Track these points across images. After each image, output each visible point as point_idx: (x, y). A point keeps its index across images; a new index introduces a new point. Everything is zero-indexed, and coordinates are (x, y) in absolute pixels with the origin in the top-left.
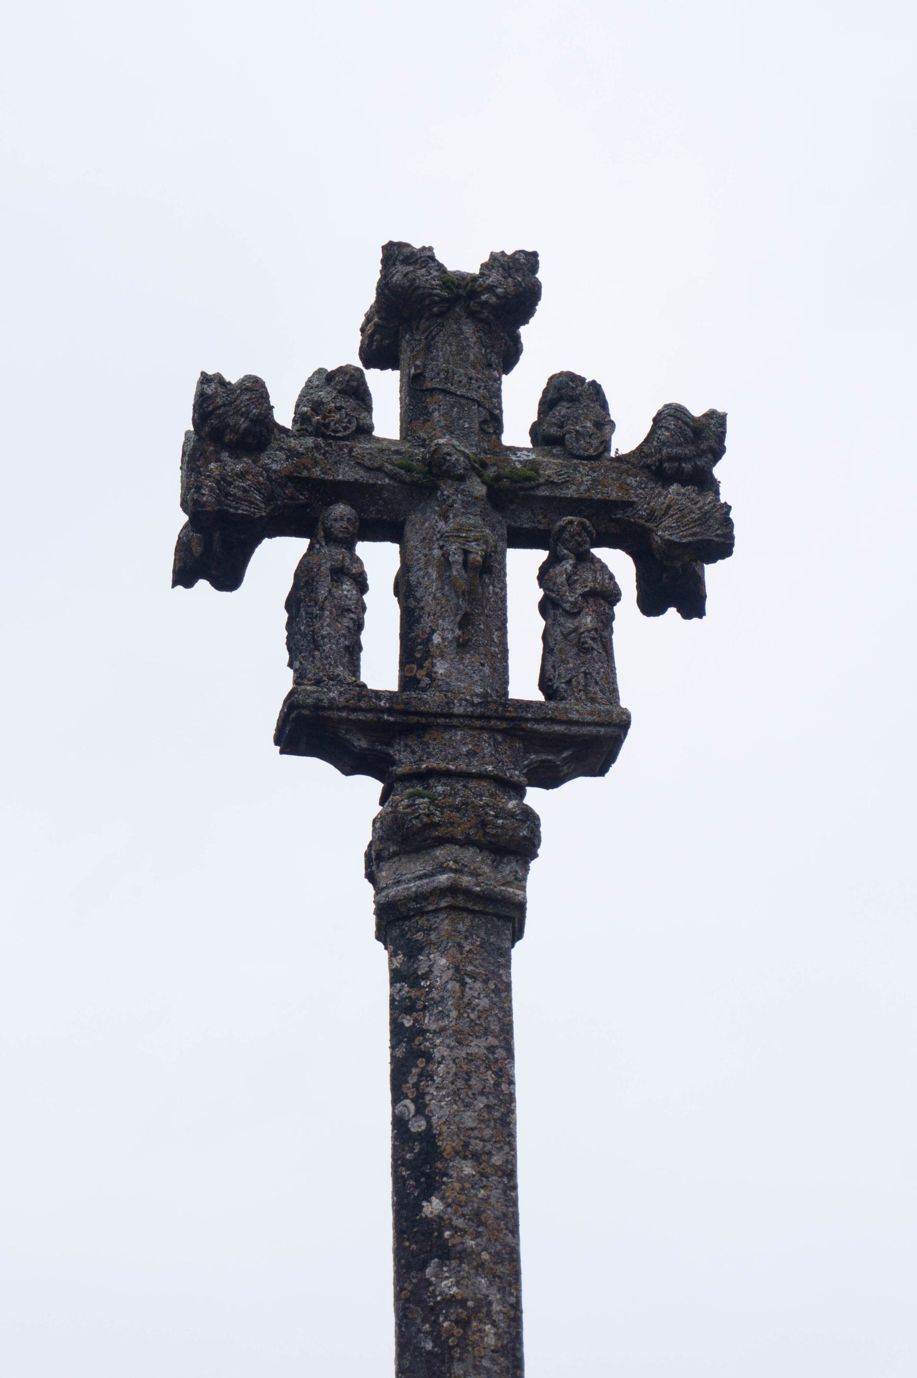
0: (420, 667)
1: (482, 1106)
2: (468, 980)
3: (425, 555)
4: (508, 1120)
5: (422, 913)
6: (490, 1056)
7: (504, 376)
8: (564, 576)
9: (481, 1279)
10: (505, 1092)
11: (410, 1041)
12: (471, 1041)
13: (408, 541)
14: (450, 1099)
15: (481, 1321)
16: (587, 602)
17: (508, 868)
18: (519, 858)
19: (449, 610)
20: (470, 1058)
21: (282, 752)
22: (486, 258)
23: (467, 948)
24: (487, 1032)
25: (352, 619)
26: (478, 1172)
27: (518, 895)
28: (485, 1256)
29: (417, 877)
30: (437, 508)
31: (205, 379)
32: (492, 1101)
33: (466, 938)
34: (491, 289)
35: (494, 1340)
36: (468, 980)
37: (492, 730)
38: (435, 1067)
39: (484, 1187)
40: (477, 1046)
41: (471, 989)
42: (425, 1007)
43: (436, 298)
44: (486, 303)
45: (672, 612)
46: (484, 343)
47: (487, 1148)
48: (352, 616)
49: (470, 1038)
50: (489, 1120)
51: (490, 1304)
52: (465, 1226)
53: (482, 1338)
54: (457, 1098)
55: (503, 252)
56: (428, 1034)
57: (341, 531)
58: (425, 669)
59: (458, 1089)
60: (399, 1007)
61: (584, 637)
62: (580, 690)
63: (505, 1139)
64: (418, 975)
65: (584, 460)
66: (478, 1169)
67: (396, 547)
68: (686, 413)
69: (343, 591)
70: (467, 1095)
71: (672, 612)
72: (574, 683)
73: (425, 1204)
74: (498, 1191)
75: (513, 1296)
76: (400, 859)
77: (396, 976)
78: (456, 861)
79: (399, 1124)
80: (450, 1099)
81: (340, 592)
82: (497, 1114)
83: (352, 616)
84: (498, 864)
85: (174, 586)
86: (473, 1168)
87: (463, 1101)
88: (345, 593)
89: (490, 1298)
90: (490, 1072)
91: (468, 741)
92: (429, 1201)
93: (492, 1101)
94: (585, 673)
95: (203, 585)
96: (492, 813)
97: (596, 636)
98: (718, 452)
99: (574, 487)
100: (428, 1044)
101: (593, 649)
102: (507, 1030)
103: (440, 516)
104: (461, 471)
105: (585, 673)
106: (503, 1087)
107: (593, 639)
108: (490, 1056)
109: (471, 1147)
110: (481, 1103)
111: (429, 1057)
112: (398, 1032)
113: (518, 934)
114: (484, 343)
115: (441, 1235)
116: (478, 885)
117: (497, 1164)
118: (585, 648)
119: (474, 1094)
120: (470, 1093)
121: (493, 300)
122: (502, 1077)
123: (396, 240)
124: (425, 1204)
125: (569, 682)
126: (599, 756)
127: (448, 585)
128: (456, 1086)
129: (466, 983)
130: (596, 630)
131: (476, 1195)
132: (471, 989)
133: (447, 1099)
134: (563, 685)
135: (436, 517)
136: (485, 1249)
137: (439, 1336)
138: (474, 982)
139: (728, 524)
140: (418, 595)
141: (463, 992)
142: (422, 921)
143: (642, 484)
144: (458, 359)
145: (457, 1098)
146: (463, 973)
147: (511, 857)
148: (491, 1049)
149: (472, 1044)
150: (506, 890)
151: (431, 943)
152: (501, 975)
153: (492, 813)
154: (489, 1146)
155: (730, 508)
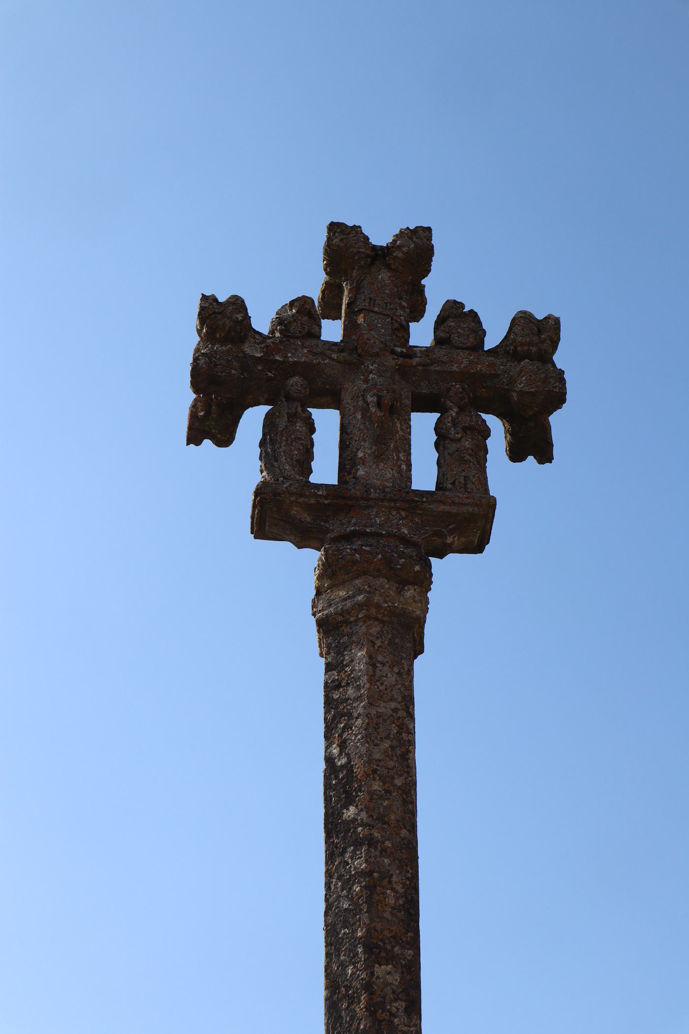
0: (349, 473)
1: (387, 745)
2: (379, 665)
3: (354, 406)
4: (407, 757)
5: (347, 622)
6: (395, 714)
7: (413, 326)
8: (450, 418)
9: (384, 859)
10: (404, 739)
11: (337, 707)
12: (380, 704)
13: (343, 400)
14: (363, 740)
15: (383, 887)
16: (466, 434)
17: (410, 592)
18: (416, 587)
19: (369, 436)
20: (379, 715)
21: (255, 538)
22: (397, 232)
23: (379, 645)
24: (392, 699)
25: (302, 444)
26: (384, 790)
27: (416, 612)
28: (388, 844)
29: (343, 600)
30: (362, 377)
31: (204, 298)
32: (395, 743)
33: (378, 638)
34: (400, 247)
35: (393, 900)
36: (379, 665)
37: (398, 509)
38: (354, 721)
39: (388, 799)
40: (385, 708)
41: (380, 670)
42: (348, 684)
43: (362, 255)
44: (396, 257)
45: (531, 459)
46: (396, 285)
47: (390, 774)
48: (302, 442)
49: (380, 702)
50: (392, 756)
51: (392, 876)
52: (373, 823)
53: (385, 898)
54: (368, 740)
55: (408, 228)
56: (349, 701)
57: (296, 392)
58: (352, 474)
59: (370, 734)
60: (329, 688)
61: (463, 453)
62: (461, 488)
63: (404, 768)
64: (343, 665)
65: (464, 350)
66: (383, 788)
67: (338, 412)
68: (531, 319)
69: (296, 427)
70: (376, 738)
71: (531, 459)
72: (457, 483)
73: (345, 811)
74: (398, 802)
75: (409, 873)
76: (332, 590)
77: (329, 668)
78: (369, 586)
79: (329, 760)
80: (363, 740)
81: (294, 428)
82: (398, 752)
83: (302, 442)
84: (401, 591)
85: (188, 444)
86: (379, 786)
87: (373, 741)
88: (298, 428)
89: (391, 873)
90: (394, 725)
91: (381, 515)
92: (348, 809)
93: (395, 743)
94: (465, 477)
95: (207, 443)
96: (395, 555)
97: (473, 453)
98: (555, 343)
99: (456, 365)
100: (349, 707)
101: (470, 461)
102: (409, 700)
103: (363, 382)
104: (377, 350)
105: (465, 477)
106: (403, 735)
107: (470, 455)
108: (395, 714)
109: (378, 773)
110: (386, 744)
111: (350, 715)
112: (329, 703)
113: (418, 648)
114: (396, 285)
115: (355, 832)
116: (386, 602)
117: (398, 785)
118: (464, 461)
119: (381, 738)
120: (378, 737)
121: (400, 255)
122: (402, 729)
123: (335, 221)
124: (345, 811)
125: (453, 483)
126: (475, 530)
127: (368, 421)
128: (368, 731)
129: (377, 667)
130: (472, 450)
131: (382, 804)
132: (380, 670)
133: (361, 741)
134: (450, 485)
135: (361, 382)
136: (388, 839)
137: (352, 899)
138: (383, 667)
139: (563, 381)
140: (349, 431)
141: (374, 672)
142: (346, 629)
143: (503, 363)
144: (378, 293)
145: (368, 740)
146: (292, 319)
147: (410, 587)
148: (395, 710)
149: (381, 706)
150: (407, 608)
151: (353, 642)
152: (403, 664)
153: (395, 555)
154: (392, 773)
155: (563, 372)
